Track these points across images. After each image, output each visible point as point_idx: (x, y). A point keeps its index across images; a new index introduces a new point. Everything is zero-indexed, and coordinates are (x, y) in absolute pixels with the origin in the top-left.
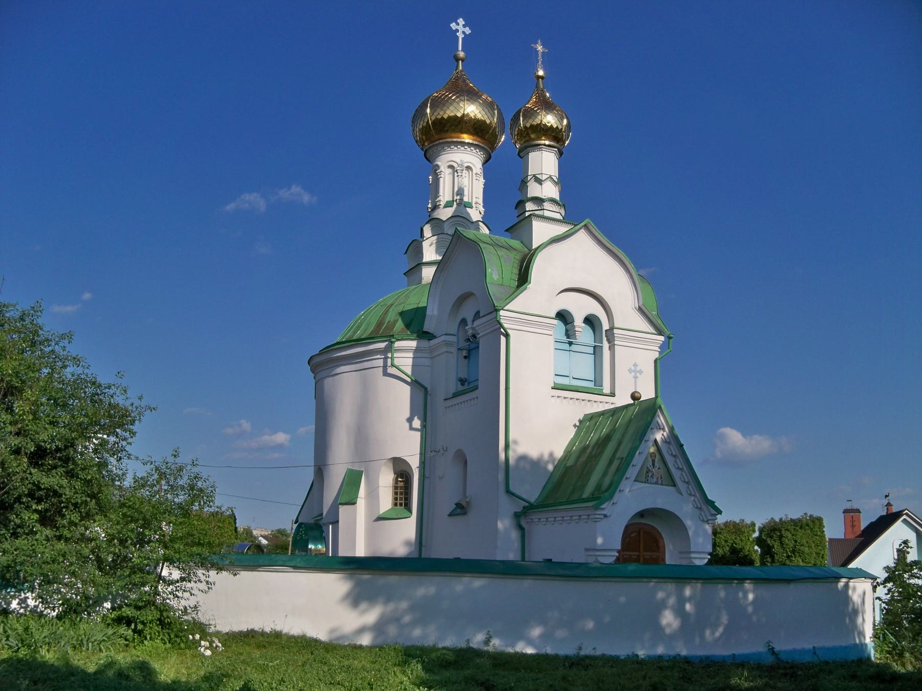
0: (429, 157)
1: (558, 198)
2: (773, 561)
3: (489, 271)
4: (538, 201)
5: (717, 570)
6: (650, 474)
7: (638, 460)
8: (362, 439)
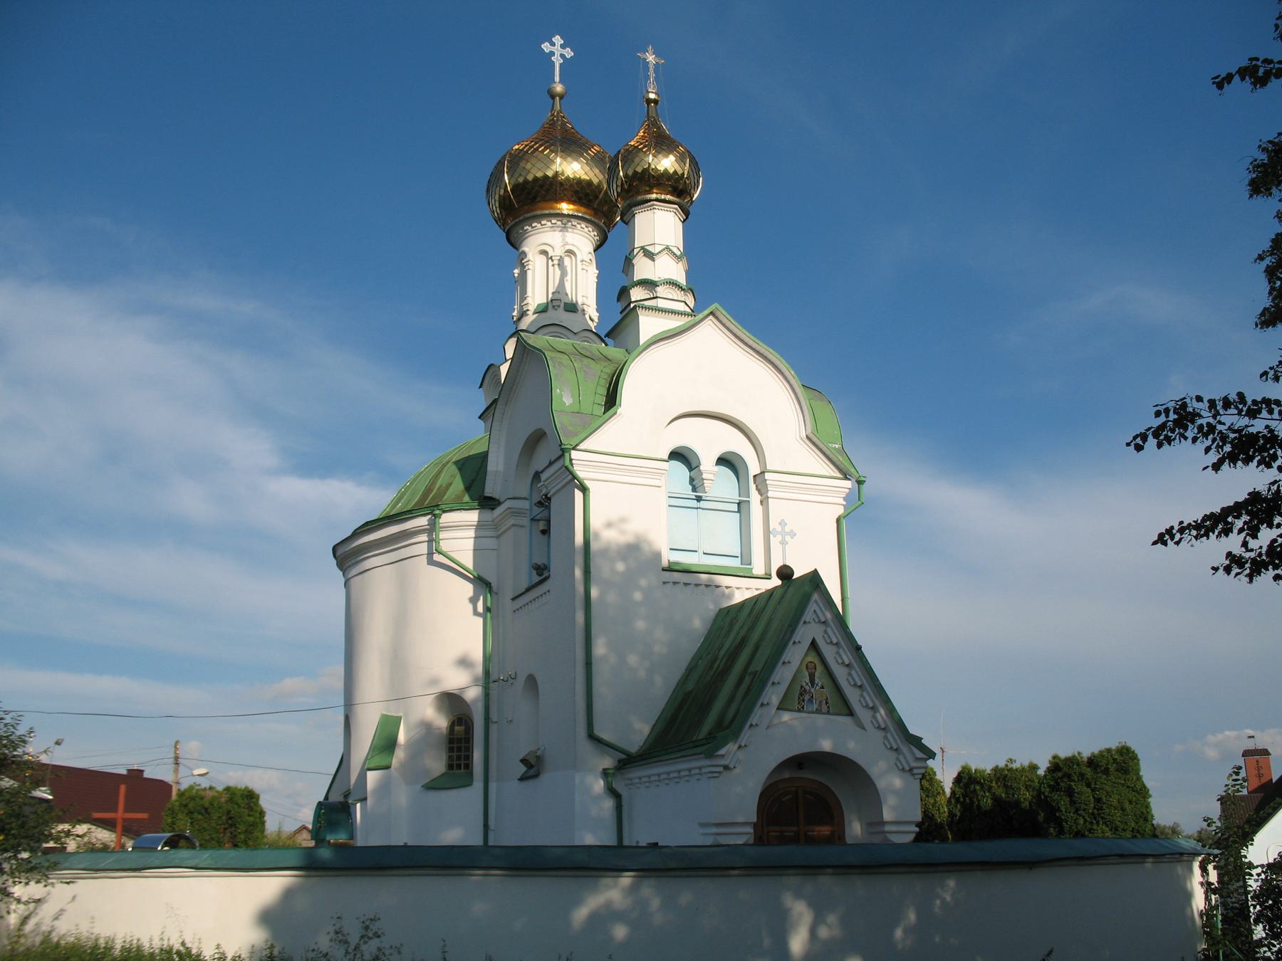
0: (514, 240)
1: (682, 280)
2: (1061, 832)
3: (556, 391)
4: (649, 284)
5: (936, 850)
6: (807, 697)
7: (784, 675)
8: (398, 663)
